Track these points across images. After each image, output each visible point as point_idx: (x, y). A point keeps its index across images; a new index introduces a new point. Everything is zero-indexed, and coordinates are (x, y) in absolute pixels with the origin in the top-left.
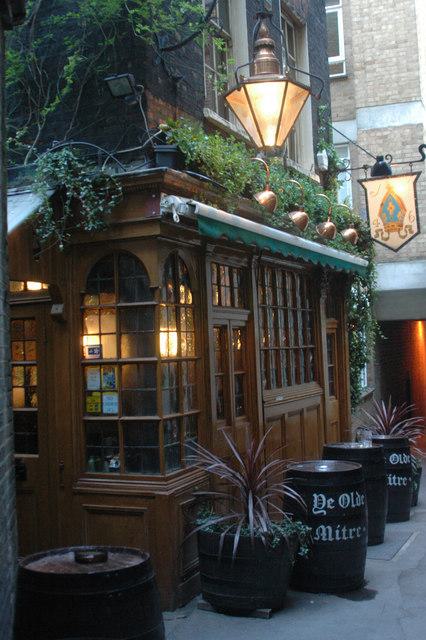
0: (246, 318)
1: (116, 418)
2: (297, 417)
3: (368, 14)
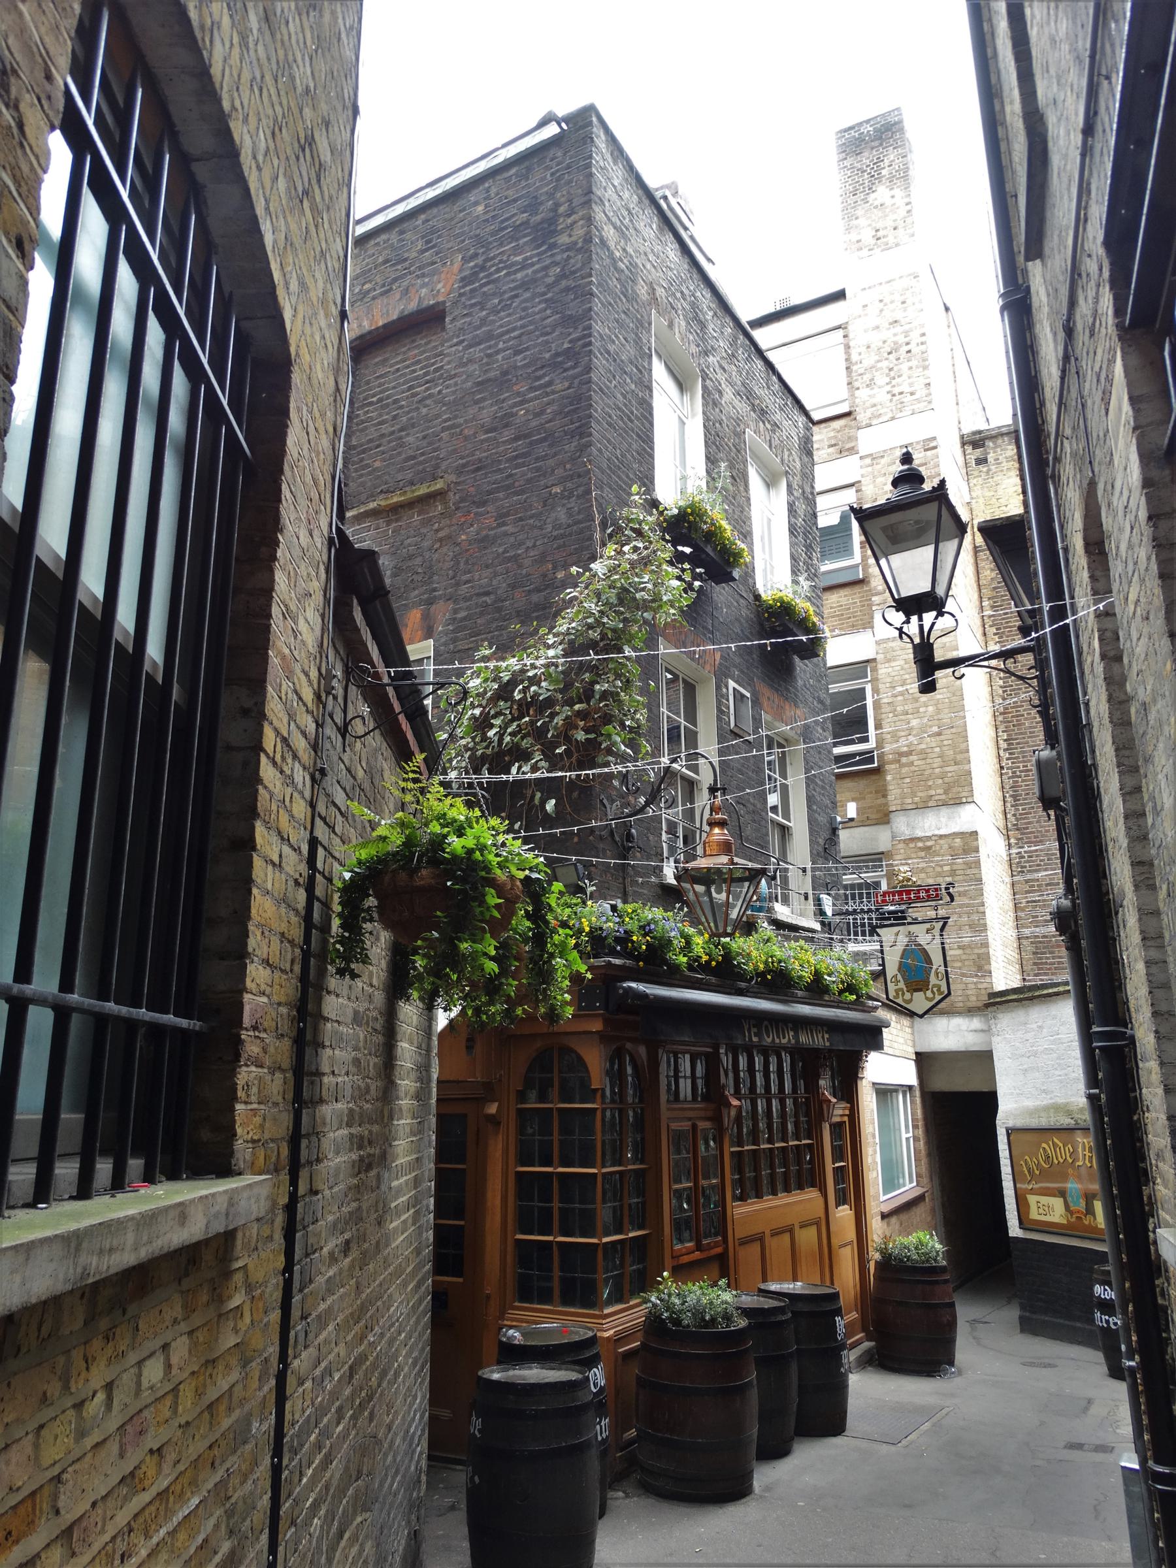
3: (901, 694)
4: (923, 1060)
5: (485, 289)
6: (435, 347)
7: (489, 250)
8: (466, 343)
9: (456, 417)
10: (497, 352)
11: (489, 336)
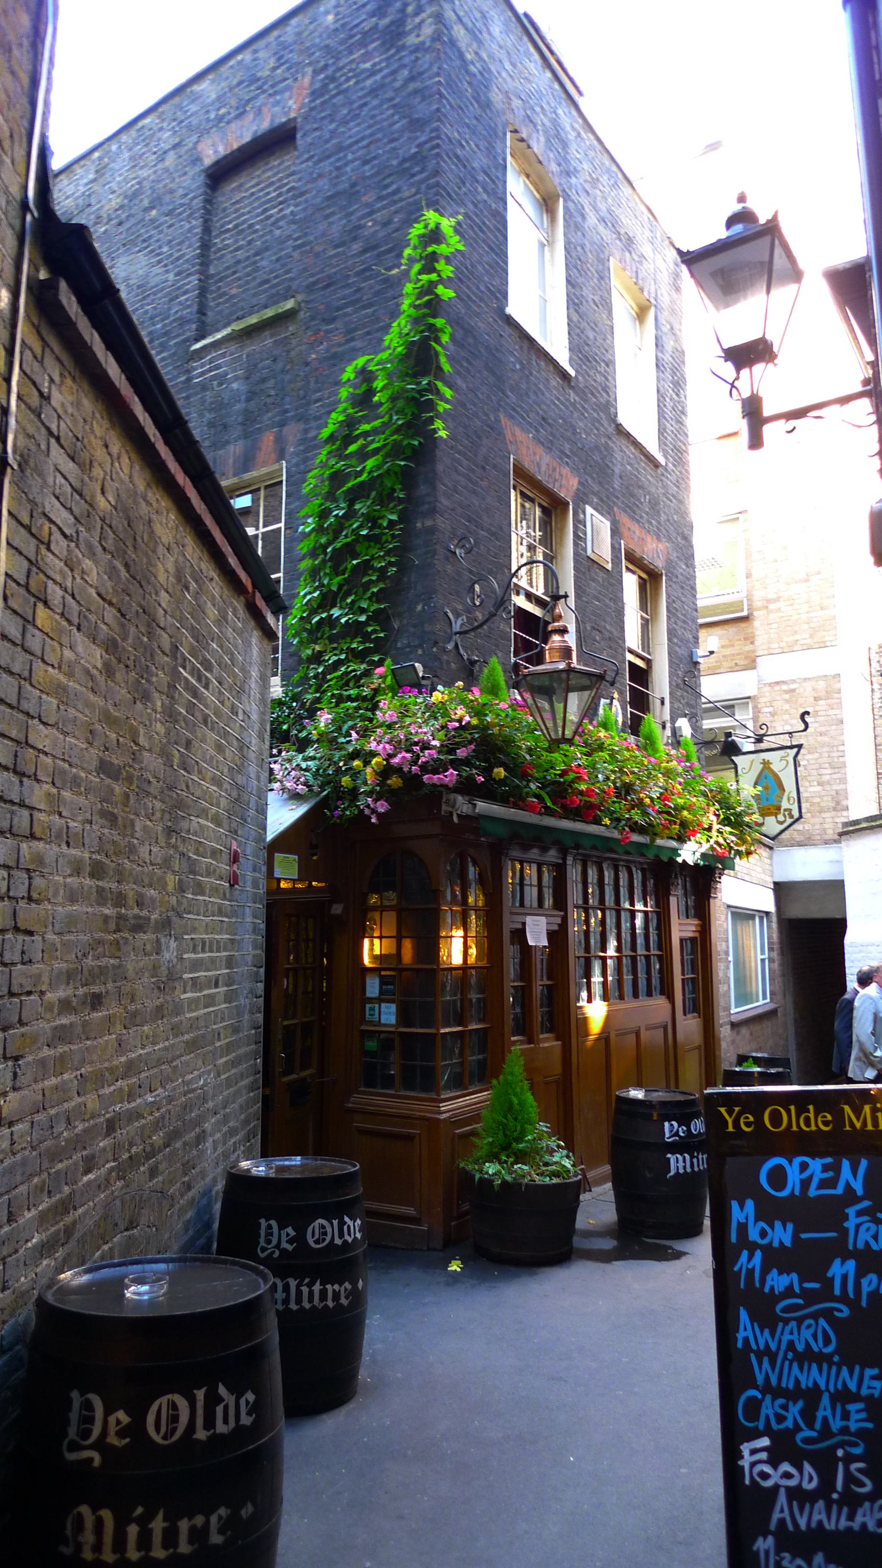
0: (559, 920)
1: (393, 1029)
2: (633, 1036)
4: (781, 889)
5: (335, 101)
6: (288, 167)
7: (338, 59)
8: (316, 158)
9: (306, 235)
10: (346, 165)
11: (340, 148)
